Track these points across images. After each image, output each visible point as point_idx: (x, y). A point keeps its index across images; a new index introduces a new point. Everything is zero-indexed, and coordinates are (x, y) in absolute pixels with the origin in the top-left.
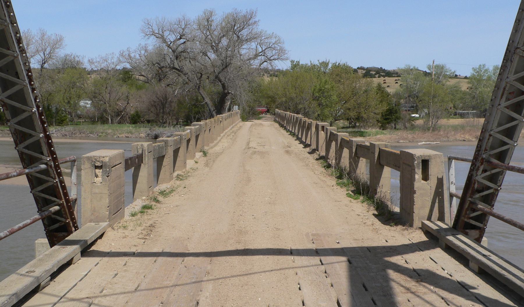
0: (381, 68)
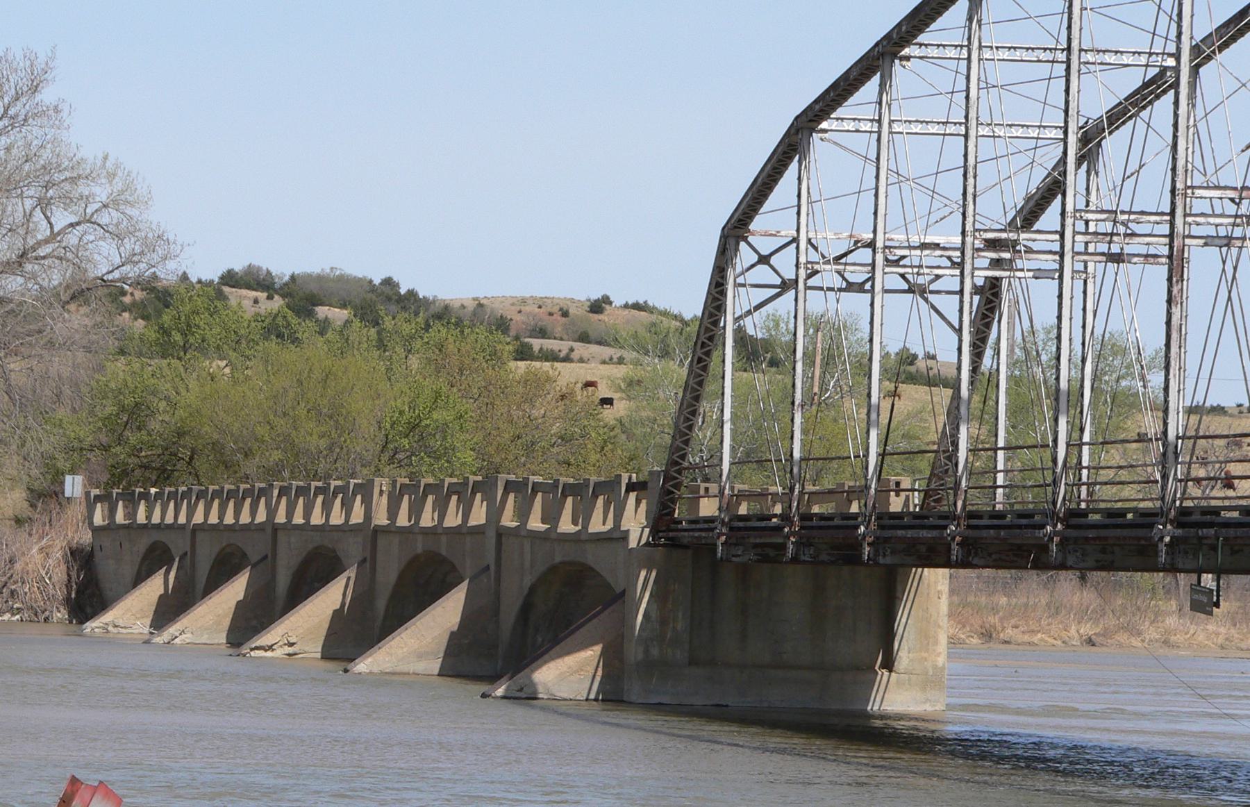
0: (388, 282)
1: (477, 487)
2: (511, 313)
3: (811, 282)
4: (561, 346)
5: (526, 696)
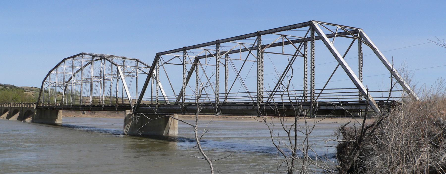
0: (13, 85)
1: (21, 103)
2: (24, 88)
3: (51, 86)
4: (29, 91)
5: (25, 122)
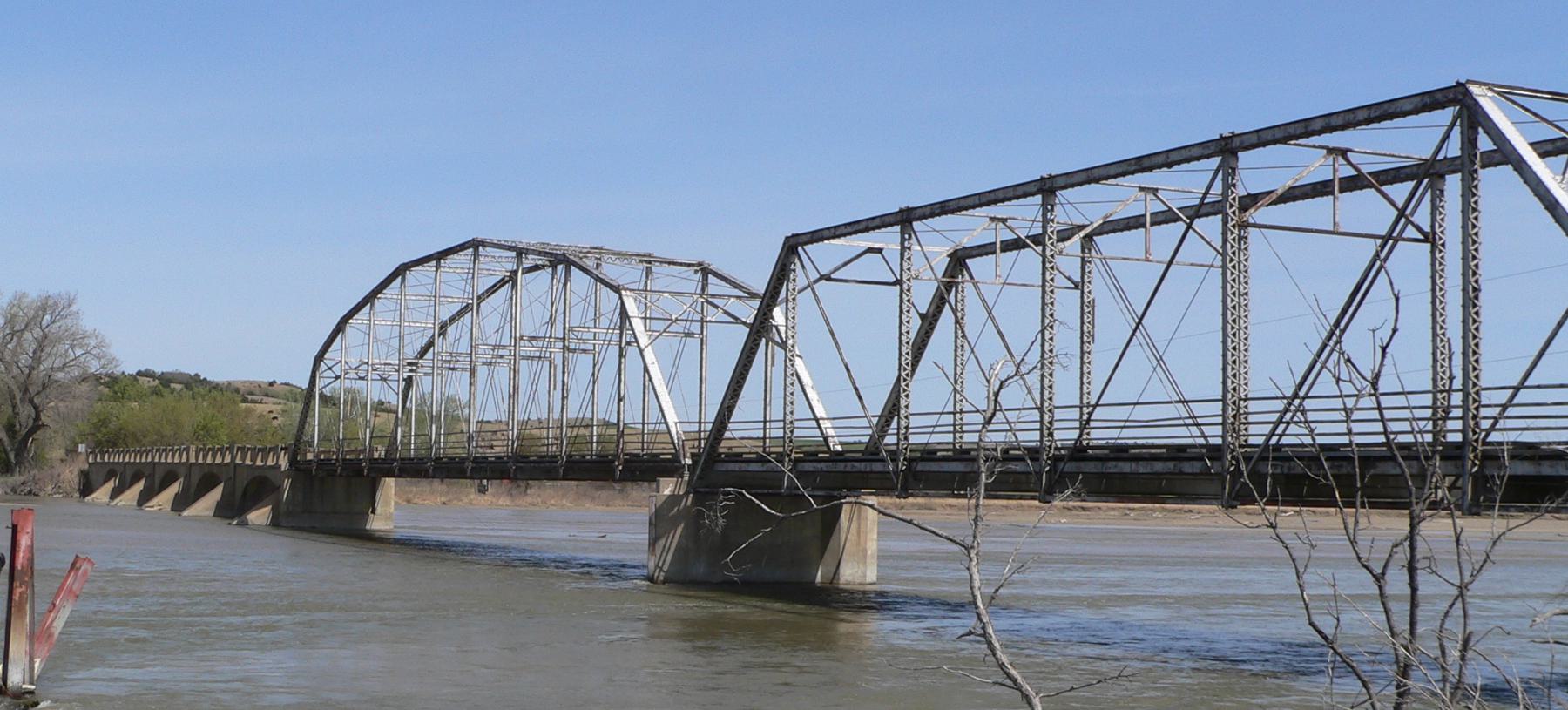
0: (196, 375)
